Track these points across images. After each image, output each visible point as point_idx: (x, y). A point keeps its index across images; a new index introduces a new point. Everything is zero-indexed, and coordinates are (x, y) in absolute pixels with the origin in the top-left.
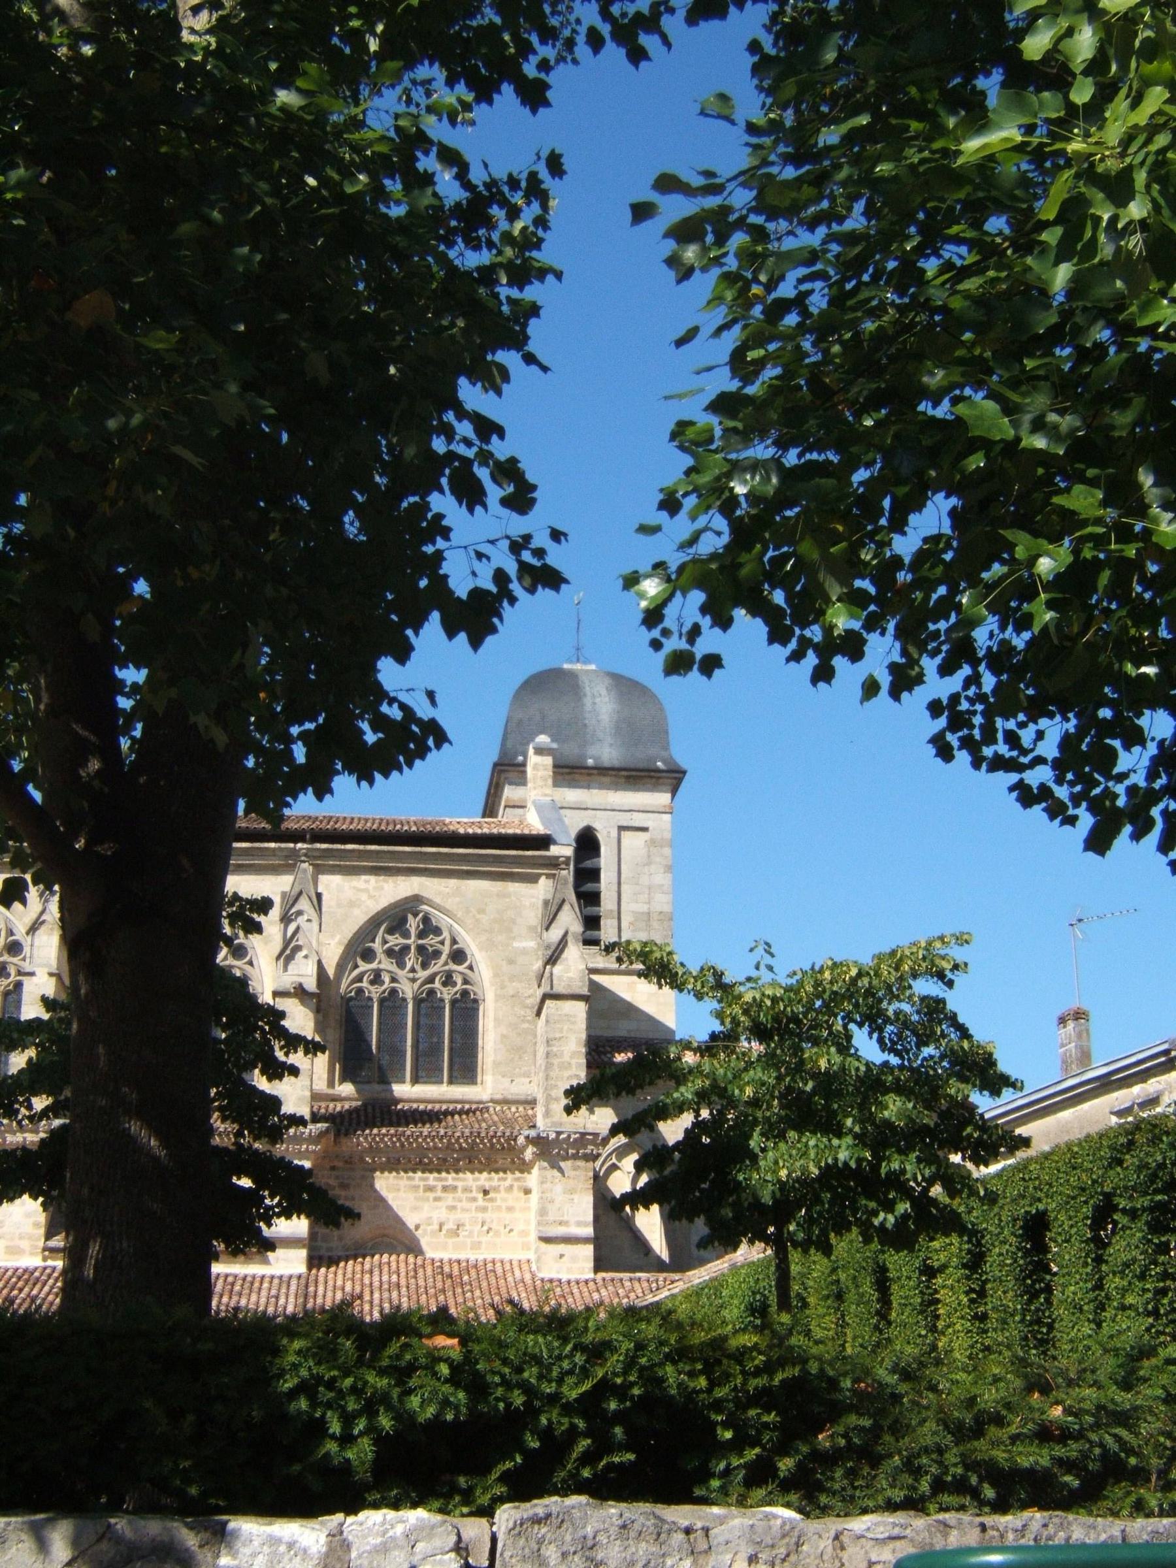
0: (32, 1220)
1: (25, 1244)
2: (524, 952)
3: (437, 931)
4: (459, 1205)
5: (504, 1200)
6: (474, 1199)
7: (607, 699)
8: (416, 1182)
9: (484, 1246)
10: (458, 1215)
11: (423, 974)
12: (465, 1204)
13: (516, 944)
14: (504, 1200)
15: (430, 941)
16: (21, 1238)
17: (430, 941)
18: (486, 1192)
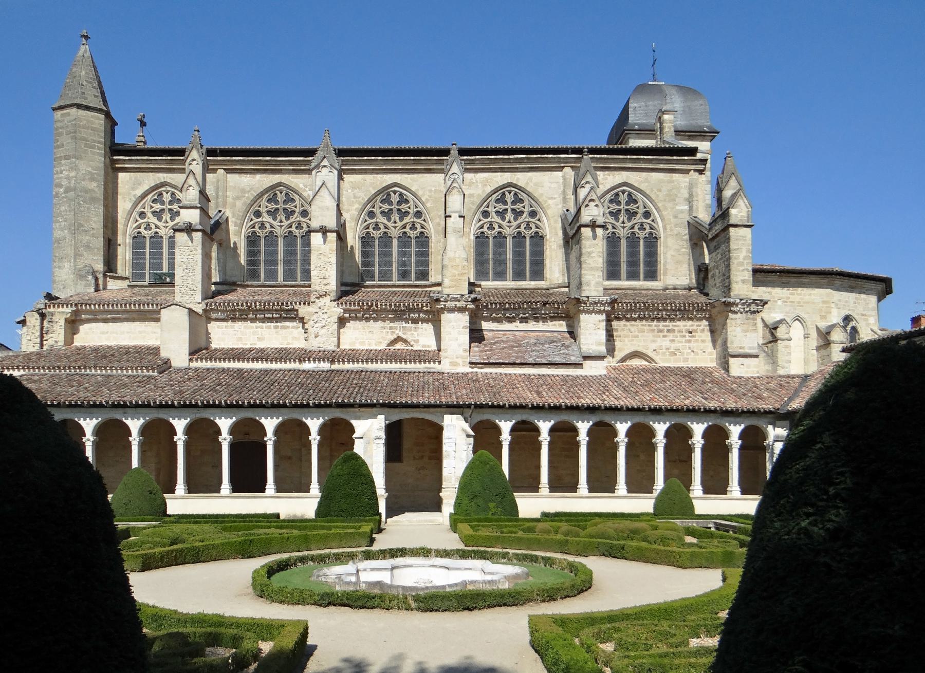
0: (462, 348)
1: (460, 361)
2: (682, 211)
3: (407, 201)
4: (676, 339)
5: (700, 337)
6: (685, 336)
7: (677, 97)
8: (653, 328)
9: (689, 360)
10: (676, 345)
11: (629, 225)
12: (679, 339)
13: (677, 208)
14: (700, 337)
15: (404, 207)
16: (457, 358)
17: (404, 207)
18: (690, 332)
